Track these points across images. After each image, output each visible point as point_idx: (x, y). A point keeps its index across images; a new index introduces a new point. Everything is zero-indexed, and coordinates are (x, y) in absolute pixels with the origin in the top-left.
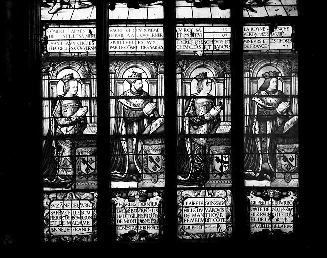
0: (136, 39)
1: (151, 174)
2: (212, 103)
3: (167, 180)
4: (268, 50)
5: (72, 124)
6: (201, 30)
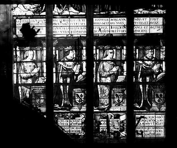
0: (150, 25)
1: (78, 104)
2: (157, 64)
3: (128, 106)
4: (108, 34)
5: (110, 75)
6: (71, 24)
